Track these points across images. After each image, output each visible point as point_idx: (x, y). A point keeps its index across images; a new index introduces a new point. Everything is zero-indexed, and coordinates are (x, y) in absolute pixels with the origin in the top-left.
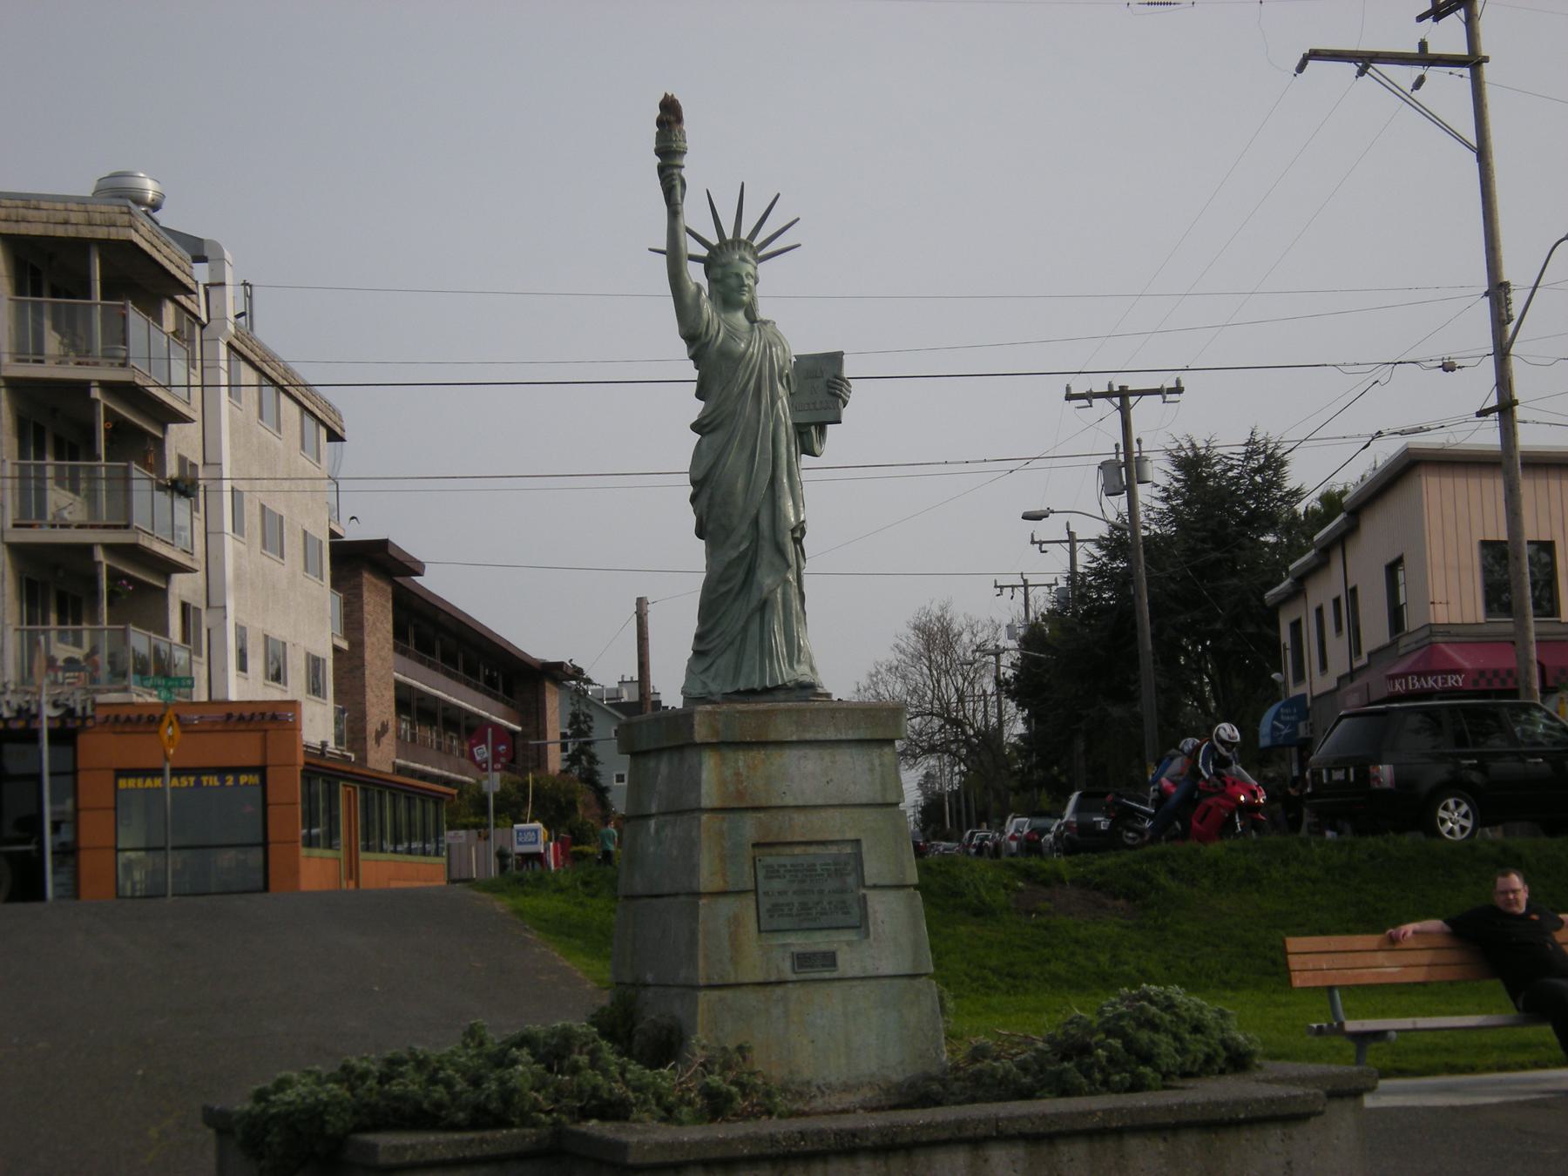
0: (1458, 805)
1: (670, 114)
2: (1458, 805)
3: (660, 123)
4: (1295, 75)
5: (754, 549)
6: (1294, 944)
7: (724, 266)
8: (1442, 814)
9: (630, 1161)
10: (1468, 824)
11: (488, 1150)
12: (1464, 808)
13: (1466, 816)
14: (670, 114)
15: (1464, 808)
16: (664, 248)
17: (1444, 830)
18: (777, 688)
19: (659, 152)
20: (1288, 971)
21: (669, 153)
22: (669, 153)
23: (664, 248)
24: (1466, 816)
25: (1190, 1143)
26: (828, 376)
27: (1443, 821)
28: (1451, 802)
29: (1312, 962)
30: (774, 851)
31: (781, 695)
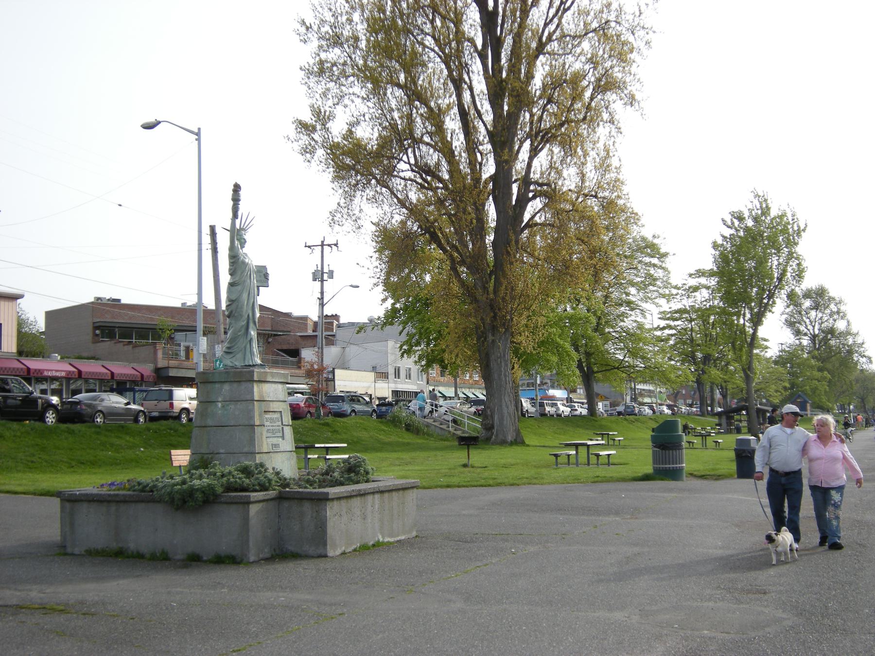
0: (53, 414)
1: (237, 188)
2: (53, 414)
4: (674, 254)
5: (248, 323)
6: (173, 452)
7: (240, 235)
8: (47, 415)
10: (54, 421)
11: (268, 497)
13: (54, 418)
14: (237, 188)
15: (54, 415)
16: (229, 229)
17: (47, 420)
18: (256, 365)
21: (236, 199)
22: (236, 199)
23: (229, 229)
24: (54, 418)
25: (401, 492)
26: (264, 273)
27: (47, 417)
28: (51, 412)
29: (179, 458)
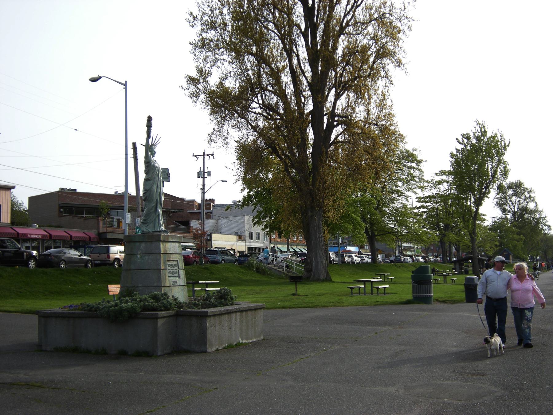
0: (33, 262)
1: (150, 119)
2: (33, 262)
3: (148, 120)
4: (426, 161)
6: (110, 286)
7: (152, 149)
8: (30, 262)
9: (208, 314)
12: (34, 263)
14: (150, 119)
15: (34, 263)
16: (145, 145)
19: (147, 126)
20: (109, 292)
23: (145, 145)
25: (253, 311)
26: (167, 173)
27: (30, 264)
28: (32, 261)
30: (169, 261)
31: (162, 232)
